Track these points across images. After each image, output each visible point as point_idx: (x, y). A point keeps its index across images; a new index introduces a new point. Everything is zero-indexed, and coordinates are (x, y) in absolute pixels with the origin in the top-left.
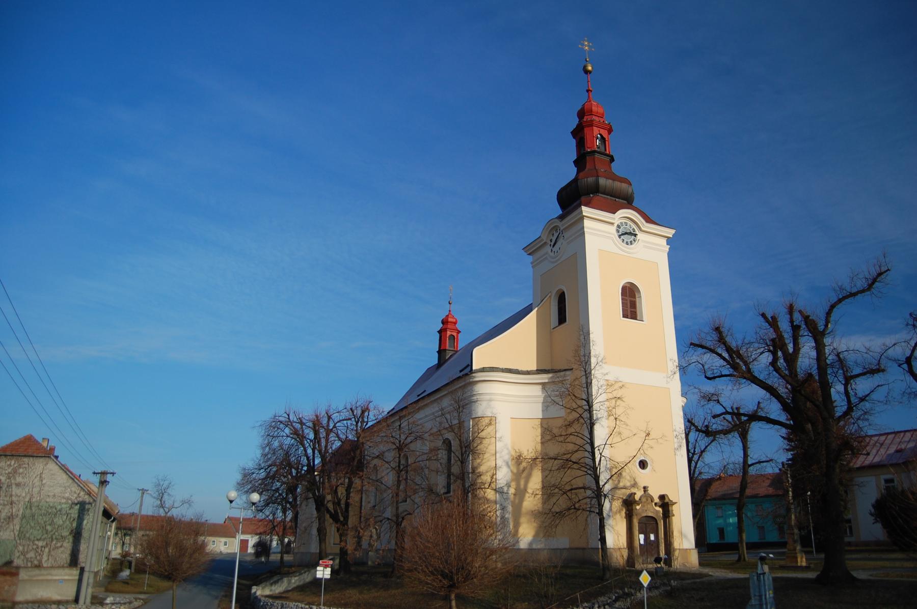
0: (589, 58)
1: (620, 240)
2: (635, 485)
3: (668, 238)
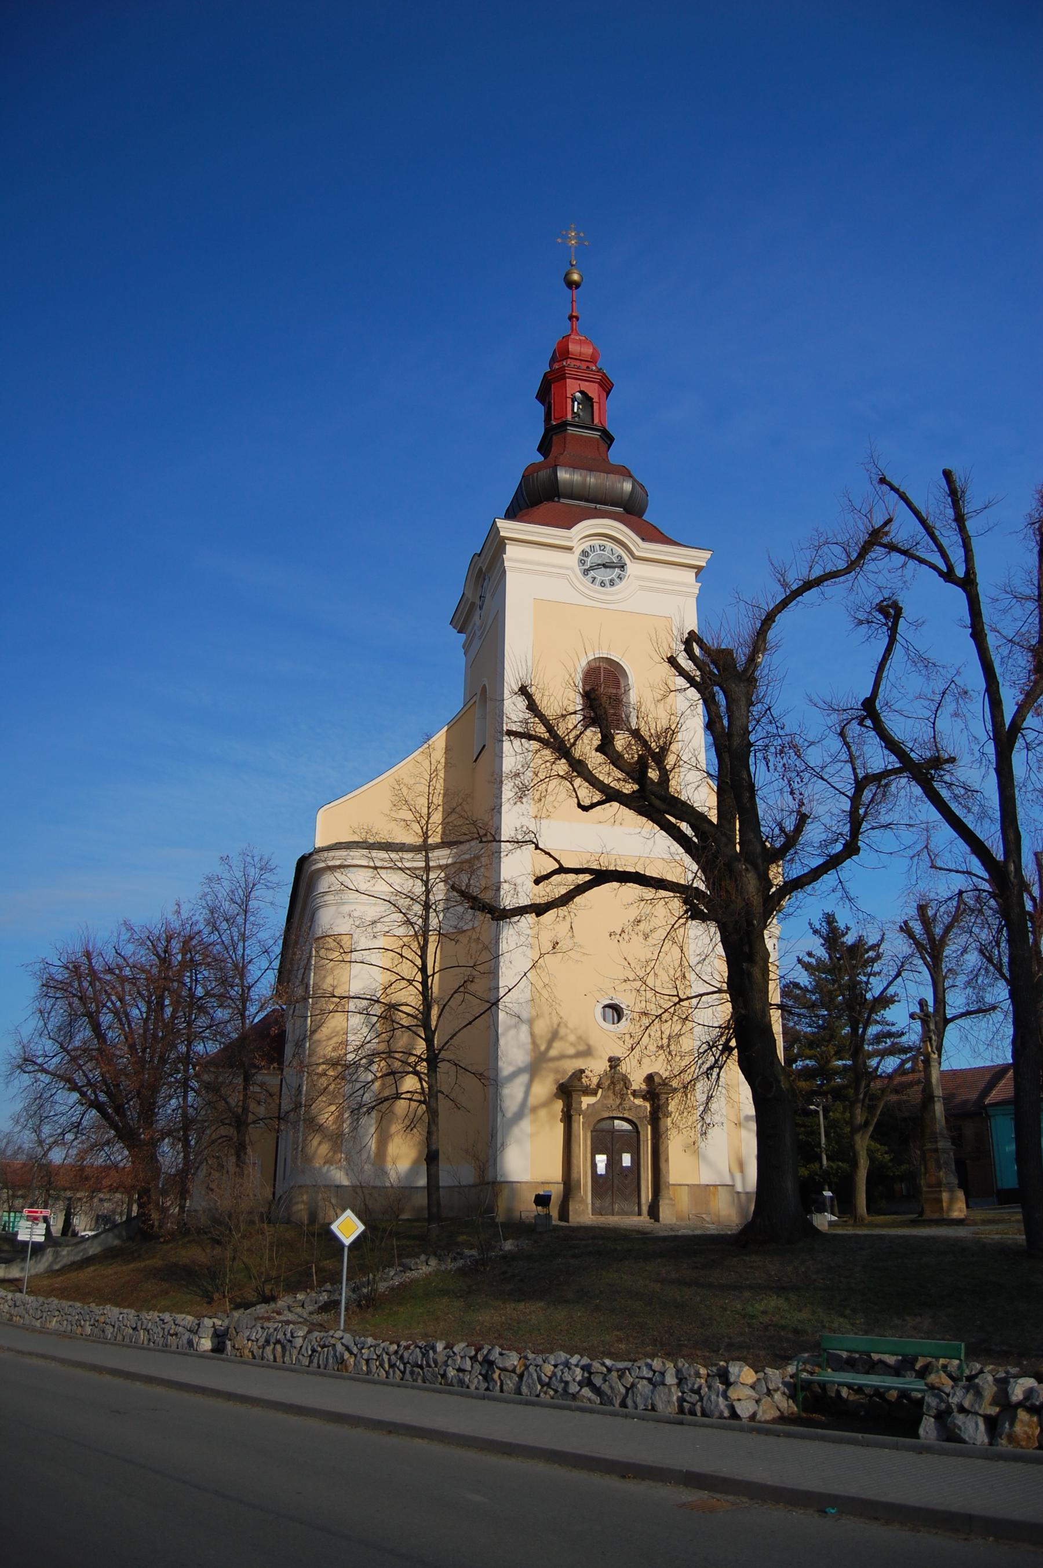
0: (576, 259)
1: (586, 581)
2: (587, 1052)
3: (699, 570)
